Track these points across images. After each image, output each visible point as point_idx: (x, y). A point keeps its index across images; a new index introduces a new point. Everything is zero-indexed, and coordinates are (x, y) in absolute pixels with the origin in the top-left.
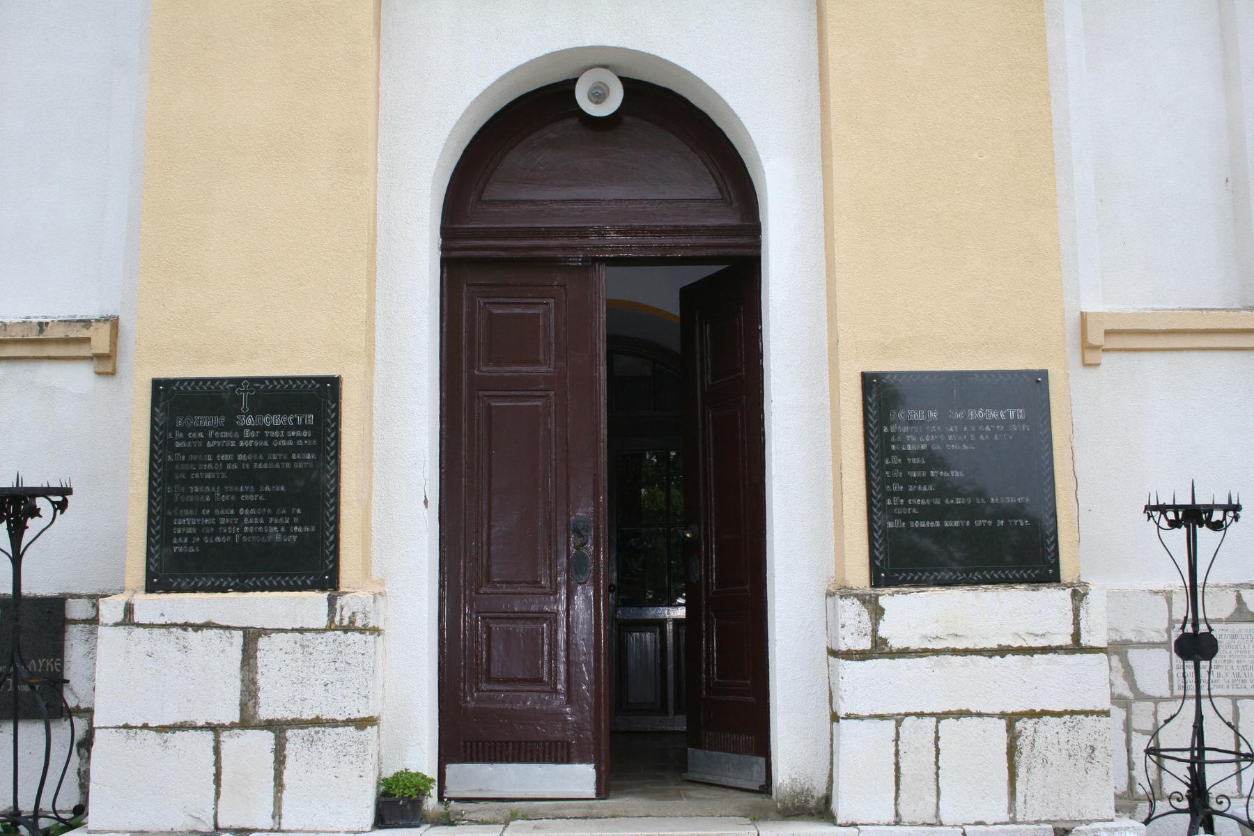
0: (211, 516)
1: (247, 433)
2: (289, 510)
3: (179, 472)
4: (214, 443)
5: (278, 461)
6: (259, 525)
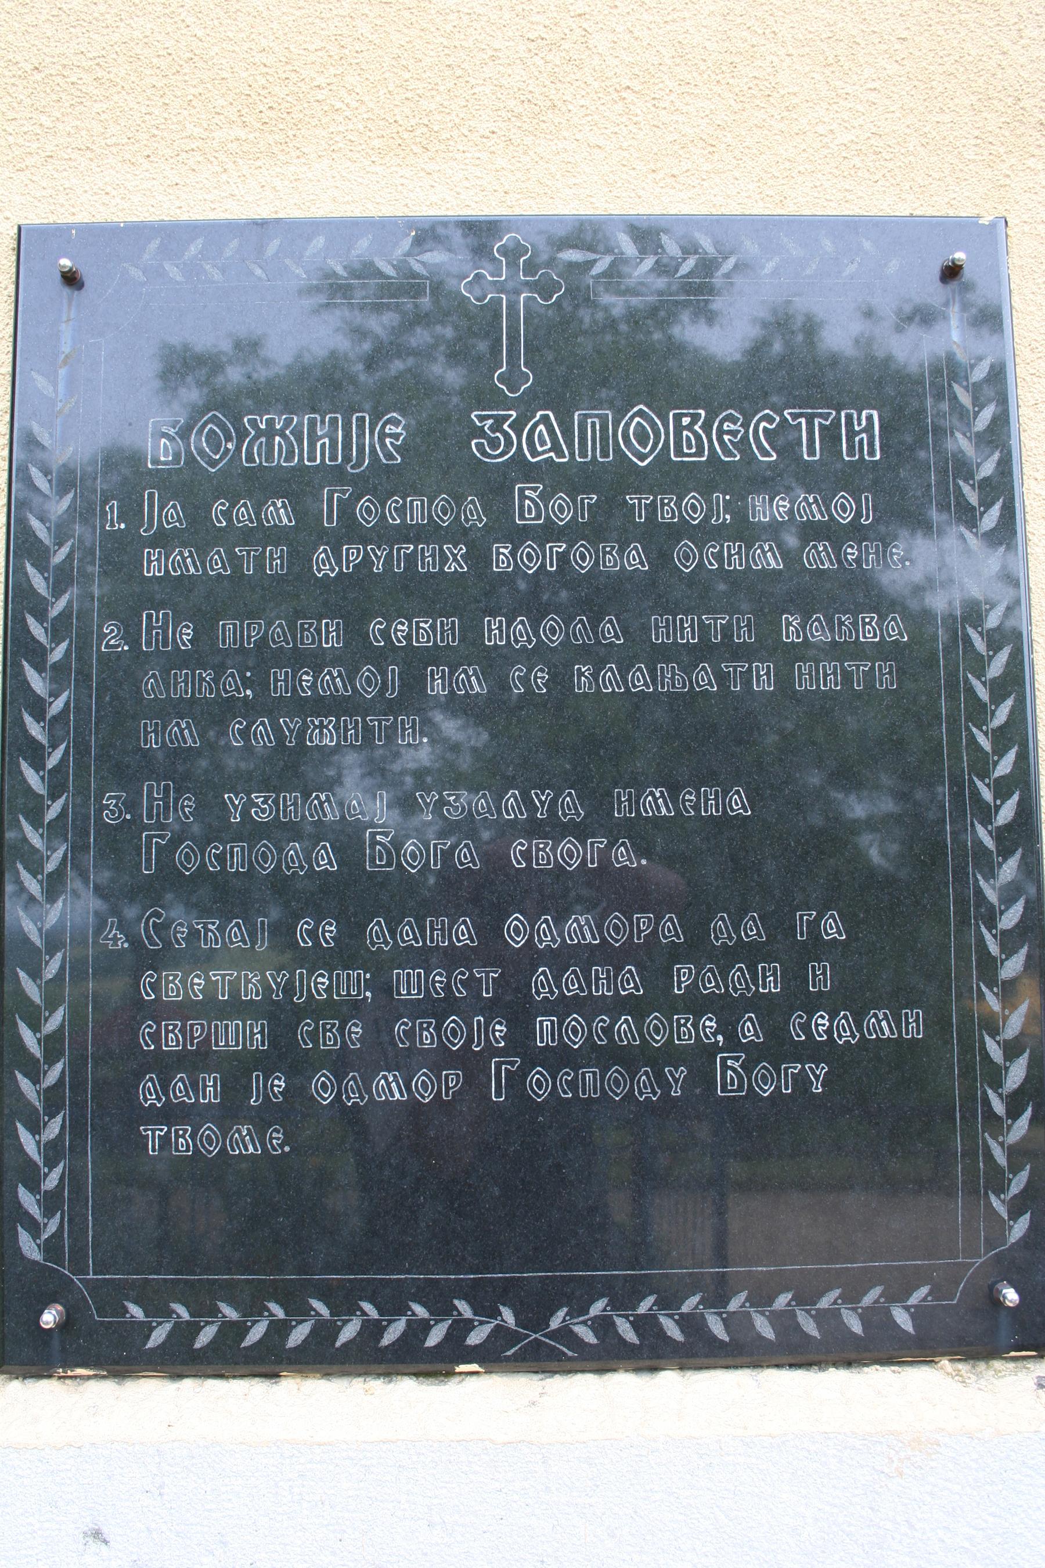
0: (347, 954)
1: (529, 502)
2: (779, 924)
3: (168, 710)
4: (353, 553)
5: (703, 651)
6: (619, 1005)
